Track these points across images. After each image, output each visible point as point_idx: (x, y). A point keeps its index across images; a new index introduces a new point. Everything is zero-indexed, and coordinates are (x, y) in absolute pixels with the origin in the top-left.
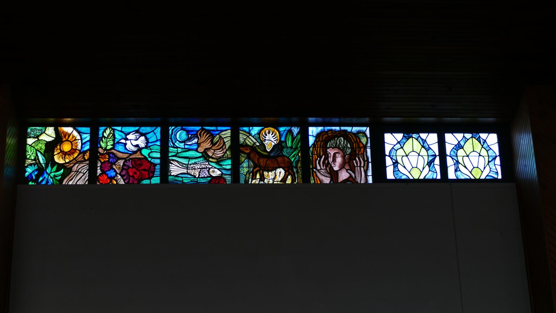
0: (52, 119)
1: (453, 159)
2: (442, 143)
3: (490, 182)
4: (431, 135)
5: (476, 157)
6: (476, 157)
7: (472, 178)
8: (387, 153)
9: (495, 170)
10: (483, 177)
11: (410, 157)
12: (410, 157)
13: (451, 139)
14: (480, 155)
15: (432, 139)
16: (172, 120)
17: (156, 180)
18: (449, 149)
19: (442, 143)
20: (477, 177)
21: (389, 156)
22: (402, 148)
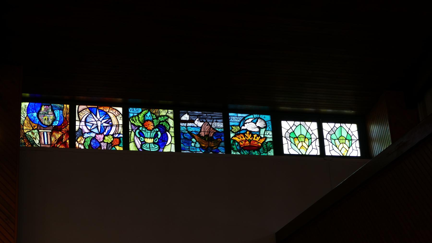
0: (28, 95)
1: (287, 139)
2: (320, 130)
3: (357, 157)
4: (353, 125)
5: (343, 140)
6: (343, 140)
7: (300, 154)
8: (283, 135)
9: (355, 151)
10: (307, 154)
11: (300, 138)
12: (300, 138)
13: (327, 127)
14: (346, 139)
15: (314, 125)
16: (231, 106)
17: (271, 153)
18: (325, 133)
19: (320, 130)
20: (304, 154)
21: (285, 137)
22: (335, 133)
